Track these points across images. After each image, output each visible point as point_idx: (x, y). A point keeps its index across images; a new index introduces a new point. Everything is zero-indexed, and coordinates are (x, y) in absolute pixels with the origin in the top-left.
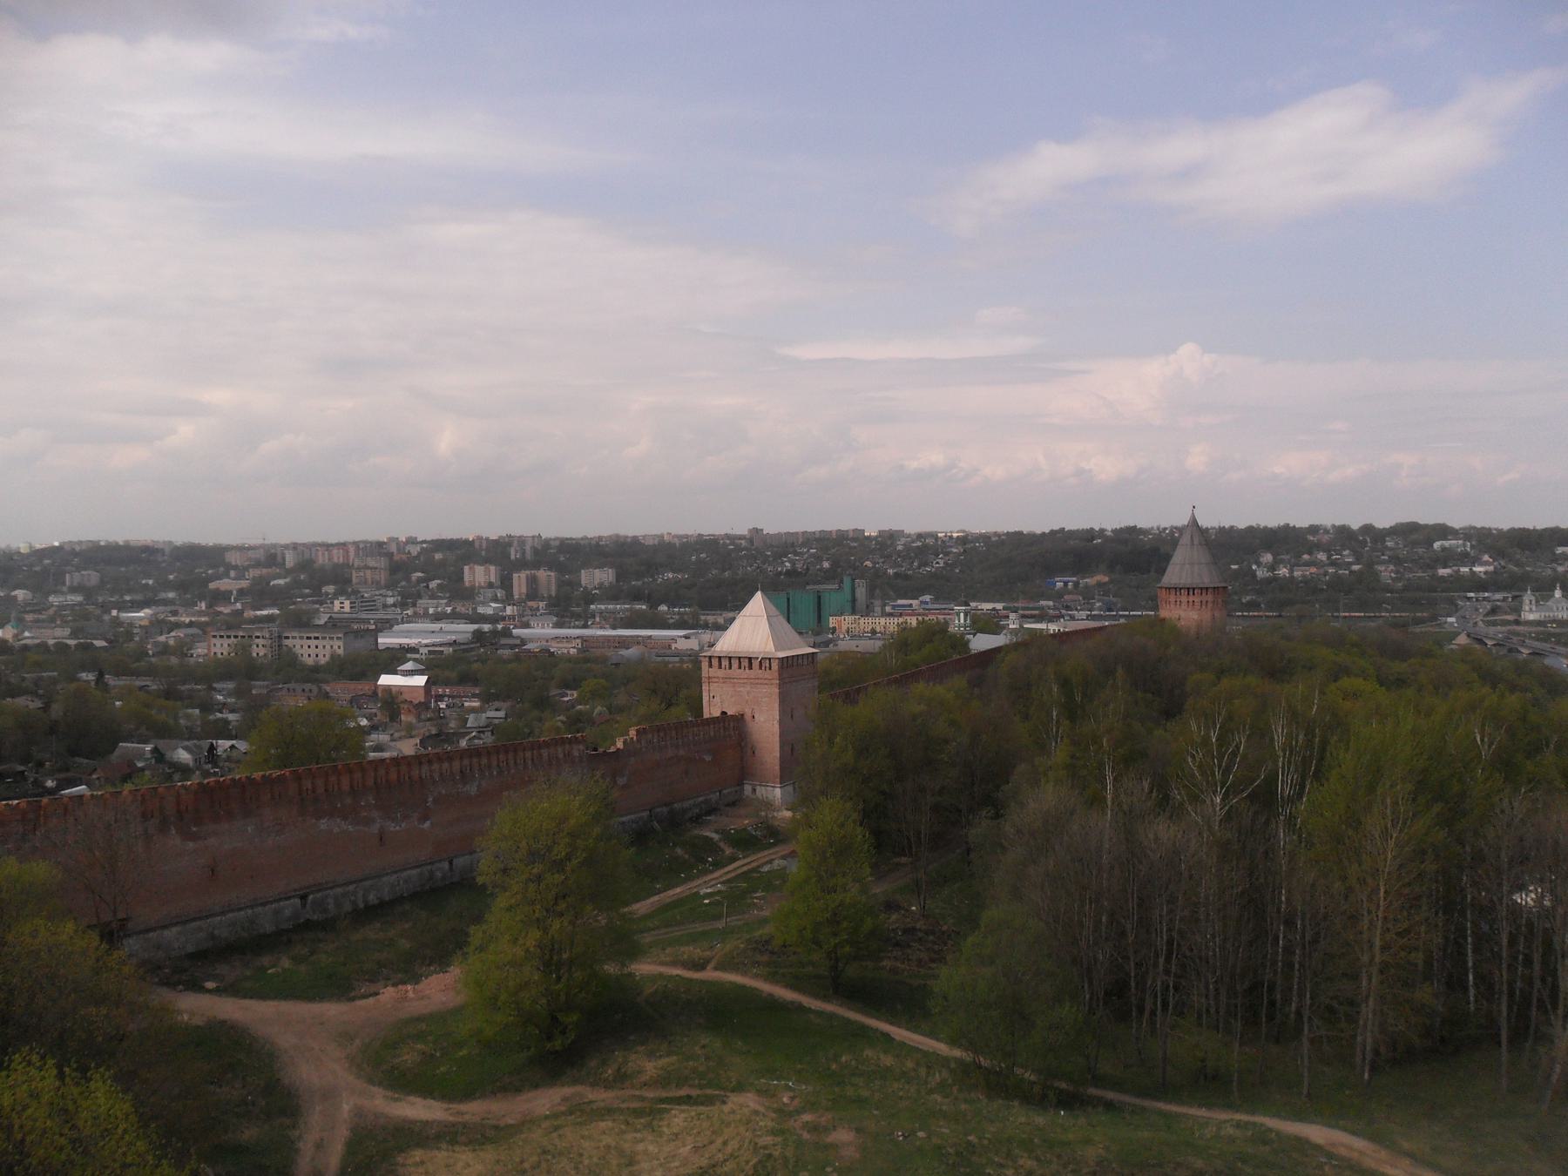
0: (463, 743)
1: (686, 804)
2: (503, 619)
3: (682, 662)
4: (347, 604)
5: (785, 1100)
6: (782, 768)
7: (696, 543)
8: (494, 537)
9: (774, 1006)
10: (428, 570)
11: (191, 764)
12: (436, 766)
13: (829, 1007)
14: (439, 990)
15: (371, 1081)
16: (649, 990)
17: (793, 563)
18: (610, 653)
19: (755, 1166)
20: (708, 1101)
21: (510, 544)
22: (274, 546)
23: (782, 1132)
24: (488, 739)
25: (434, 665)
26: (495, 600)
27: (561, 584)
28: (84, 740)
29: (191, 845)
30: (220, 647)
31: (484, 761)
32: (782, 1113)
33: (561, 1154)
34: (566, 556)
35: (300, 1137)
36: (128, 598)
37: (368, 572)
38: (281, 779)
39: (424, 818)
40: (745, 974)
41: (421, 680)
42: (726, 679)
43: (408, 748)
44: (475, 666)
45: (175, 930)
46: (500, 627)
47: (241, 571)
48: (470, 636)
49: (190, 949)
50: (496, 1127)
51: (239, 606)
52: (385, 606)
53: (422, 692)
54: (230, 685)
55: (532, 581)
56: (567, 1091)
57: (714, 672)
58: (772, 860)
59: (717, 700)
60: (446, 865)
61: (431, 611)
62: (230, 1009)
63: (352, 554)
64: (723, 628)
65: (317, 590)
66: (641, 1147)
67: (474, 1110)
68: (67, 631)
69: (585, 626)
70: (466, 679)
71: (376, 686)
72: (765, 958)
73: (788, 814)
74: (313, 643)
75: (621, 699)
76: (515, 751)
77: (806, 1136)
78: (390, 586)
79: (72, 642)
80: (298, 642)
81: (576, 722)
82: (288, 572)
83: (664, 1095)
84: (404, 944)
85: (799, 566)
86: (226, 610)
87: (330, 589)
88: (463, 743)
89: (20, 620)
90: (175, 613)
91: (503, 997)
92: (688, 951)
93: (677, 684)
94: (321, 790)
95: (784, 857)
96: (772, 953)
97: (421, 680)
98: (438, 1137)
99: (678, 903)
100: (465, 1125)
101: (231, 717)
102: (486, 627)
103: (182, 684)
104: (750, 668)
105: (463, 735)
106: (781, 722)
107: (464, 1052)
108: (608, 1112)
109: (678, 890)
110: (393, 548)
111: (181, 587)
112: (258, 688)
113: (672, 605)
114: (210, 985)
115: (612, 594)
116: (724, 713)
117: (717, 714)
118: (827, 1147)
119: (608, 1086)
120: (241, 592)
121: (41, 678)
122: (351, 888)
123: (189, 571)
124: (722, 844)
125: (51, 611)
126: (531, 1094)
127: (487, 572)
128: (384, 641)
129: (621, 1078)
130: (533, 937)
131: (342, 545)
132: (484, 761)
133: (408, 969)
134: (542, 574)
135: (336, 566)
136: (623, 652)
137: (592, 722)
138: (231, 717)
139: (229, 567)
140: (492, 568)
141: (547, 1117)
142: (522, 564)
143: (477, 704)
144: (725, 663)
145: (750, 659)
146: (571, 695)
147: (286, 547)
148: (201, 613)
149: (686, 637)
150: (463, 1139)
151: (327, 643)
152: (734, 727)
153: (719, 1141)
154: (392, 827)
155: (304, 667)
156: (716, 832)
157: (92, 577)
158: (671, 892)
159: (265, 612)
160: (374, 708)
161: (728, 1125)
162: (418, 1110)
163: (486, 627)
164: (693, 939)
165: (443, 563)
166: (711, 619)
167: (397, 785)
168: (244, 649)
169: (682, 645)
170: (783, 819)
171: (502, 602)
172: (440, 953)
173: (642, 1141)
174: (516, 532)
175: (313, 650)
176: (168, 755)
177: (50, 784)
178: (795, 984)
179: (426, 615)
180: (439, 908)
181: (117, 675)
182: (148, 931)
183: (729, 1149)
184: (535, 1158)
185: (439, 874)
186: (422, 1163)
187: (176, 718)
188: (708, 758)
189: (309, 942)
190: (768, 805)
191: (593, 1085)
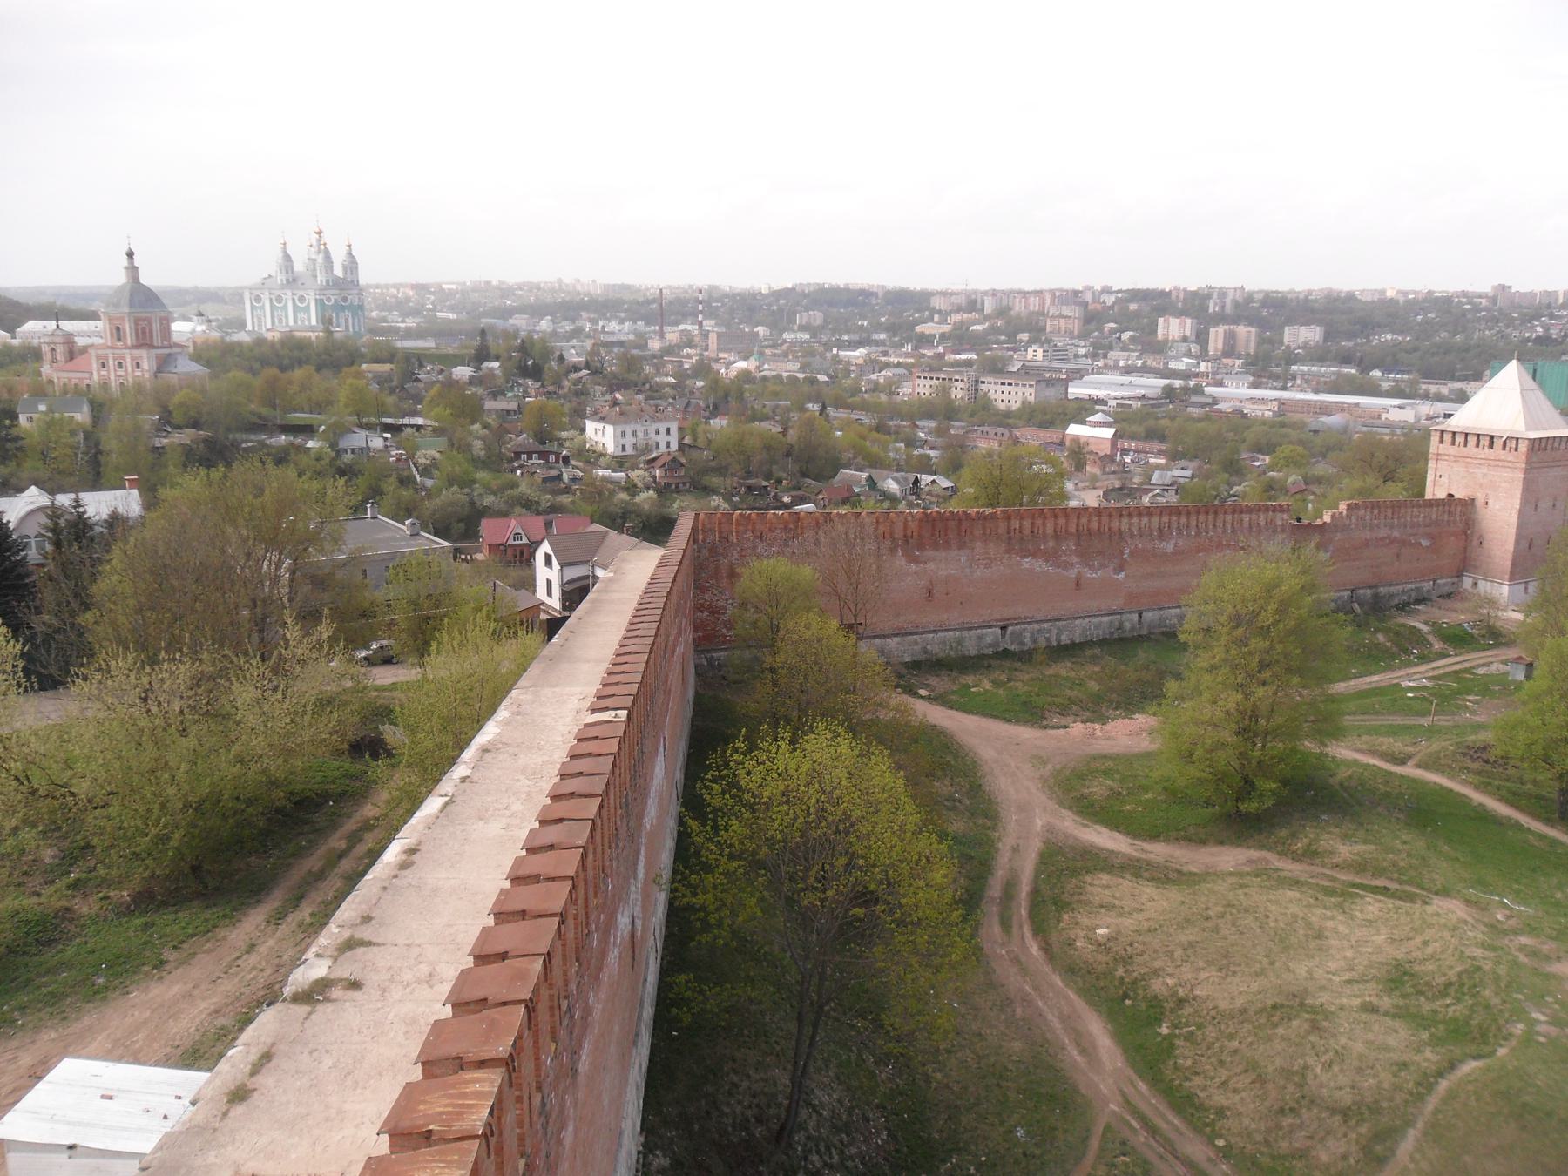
0: (1146, 500)
1: (1393, 589)
2: (1196, 375)
3: (1393, 434)
4: (1040, 352)
5: (1499, 917)
6: (1514, 564)
7: (1425, 300)
8: (1193, 288)
9: (1483, 817)
10: (1126, 320)
11: (898, 493)
12: (1135, 520)
13: (1553, 833)
14: (1128, 734)
15: (1061, 804)
16: (1343, 774)
17: (1547, 328)
18: (1308, 419)
19: (1460, 975)
20: (1410, 898)
21: (1209, 296)
22: (975, 292)
23: (1494, 949)
24: (1172, 498)
25: (1124, 419)
26: (1189, 354)
27: (1261, 341)
28: (813, 464)
29: (913, 567)
30: (923, 388)
31: (1183, 520)
32: (1494, 927)
33: (1246, 911)
34: (1271, 311)
35: (999, 839)
36: (846, 338)
37: (1062, 321)
38: (993, 516)
39: (1121, 569)
40: (1452, 778)
41: (1108, 433)
42: (1457, 458)
43: (1091, 499)
44: (1163, 422)
45: (897, 639)
46: (1192, 383)
47: (944, 315)
48: (1159, 391)
49: (907, 659)
50: (1179, 872)
51: (940, 349)
52: (1076, 356)
53: (1109, 445)
54: (932, 424)
55: (1230, 337)
56: (1254, 854)
57: (1446, 448)
58: (1491, 663)
59: (1442, 480)
60: (1135, 617)
61: (1122, 363)
62: (938, 716)
63: (1048, 301)
64: (1462, 398)
65: (1012, 337)
66: (1330, 924)
67: (1158, 851)
68: (798, 366)
69: (1284, 388)
70: (1154, 435)
71: (1064, 435)
72: (1476, 766)
73: (1519, 616)
74: (1006, 388)
75: (1321, 469)
76: (1216, 513)
77: (1522, 958)
78: (1083, 336)
79: (801, 376)
80: (992, 387)
81: (1271, 488)
82: (987, 318)
83: (1358, 880)
84: (1094, 686)
85: (1554, 332)
86: (929, 353)
87: (1024, 336)
88: (1146, 500)
89: (761, 354)
90: (885, 354)
91: (1199, 752)
92: (1386, 743)
93: (1401, 459)
94: (1027, 532)
95: (1505, 662)
96: (1487, 762)
97: (1108, 433)
98: (1123, 868)
99: (1377, 691)
100: (1148, 863)
101: (933, 453)
102: (1178, 383)
103: (892, 419)
104: (1491, 446)
105: (1147, 491)
106: (1521, 513)
107: (1149, 796)
108: (1296, 883)
109: (1376, 678)
110: (1088, 297)
111: (892, 329)
112: (956, 429)
113: (1387, 370)
114: (923, 692)
115: (1318, 355)
116: (1451, 495)
117: (1442, 495)
118: (1549, 976)
119: (1297, 858)
120: (943, 336)
121: (777, 406)
122: (1046, 625)
123: (900, 313)
124: (1431, 638)
125: (785, 347)
126: (1215, 849)
127: (1183, 326)
128: (1075, 391)
129: (1310, 855)
130: (1232, 699)
131: (1040, 293)
132: (1183, 520)
133: (1095, 709)
134: (1242, 330)
135: (1032, 313)
136: (1324, 419)
137: (1284, 490)
138: (933, 453)
139: (933, 311)
140: (1188, 321)
141: (1231, 874)
142: (1220, 318)
143: (1163, 461)
144: (1460, 439)
145: (1492, 437)
146: (1263, 460)
147: (986, 293)
148: (907, 355)
149: (1401, 407)
150: (1146, 874)
151: (1020, 390)
152: (1459, 516)
153: (1419, 940)
154: (1089, 574)
155: (997, 412)
156: (1426, 623)
157: (817, 317)
158: (1367, 679)
159: (963, 357)
160: (1062, 456)
161: (1431, 926)
162: (1102, 838)
163: (1178, 383)
164: (1393, 731)
165: (1137, 314)
166: (1433, 389)
167: (1095, 534)
168: (945, 391)
169: (1395, 416)
170: (1508, 620)
171: (1196, 357)
172: (1131, 699)
173: (1332, 918)
174: (1217, 284)
175: (1007, 396)
176: (880, 485)
177: (786, 499)
178: (1513, 799)
179: (1116, 367)
180: (1132, 660)
181: (836, 407)
182: (875, 637)
183: (1429, 950)
184: (1221, 909)
185: (1128, 625)
186: (1108, 887)
187: (885, 448)
188: (1425, 543)
189: (1017, 668)
190: (1491, 602)
191: (1281, 854)
